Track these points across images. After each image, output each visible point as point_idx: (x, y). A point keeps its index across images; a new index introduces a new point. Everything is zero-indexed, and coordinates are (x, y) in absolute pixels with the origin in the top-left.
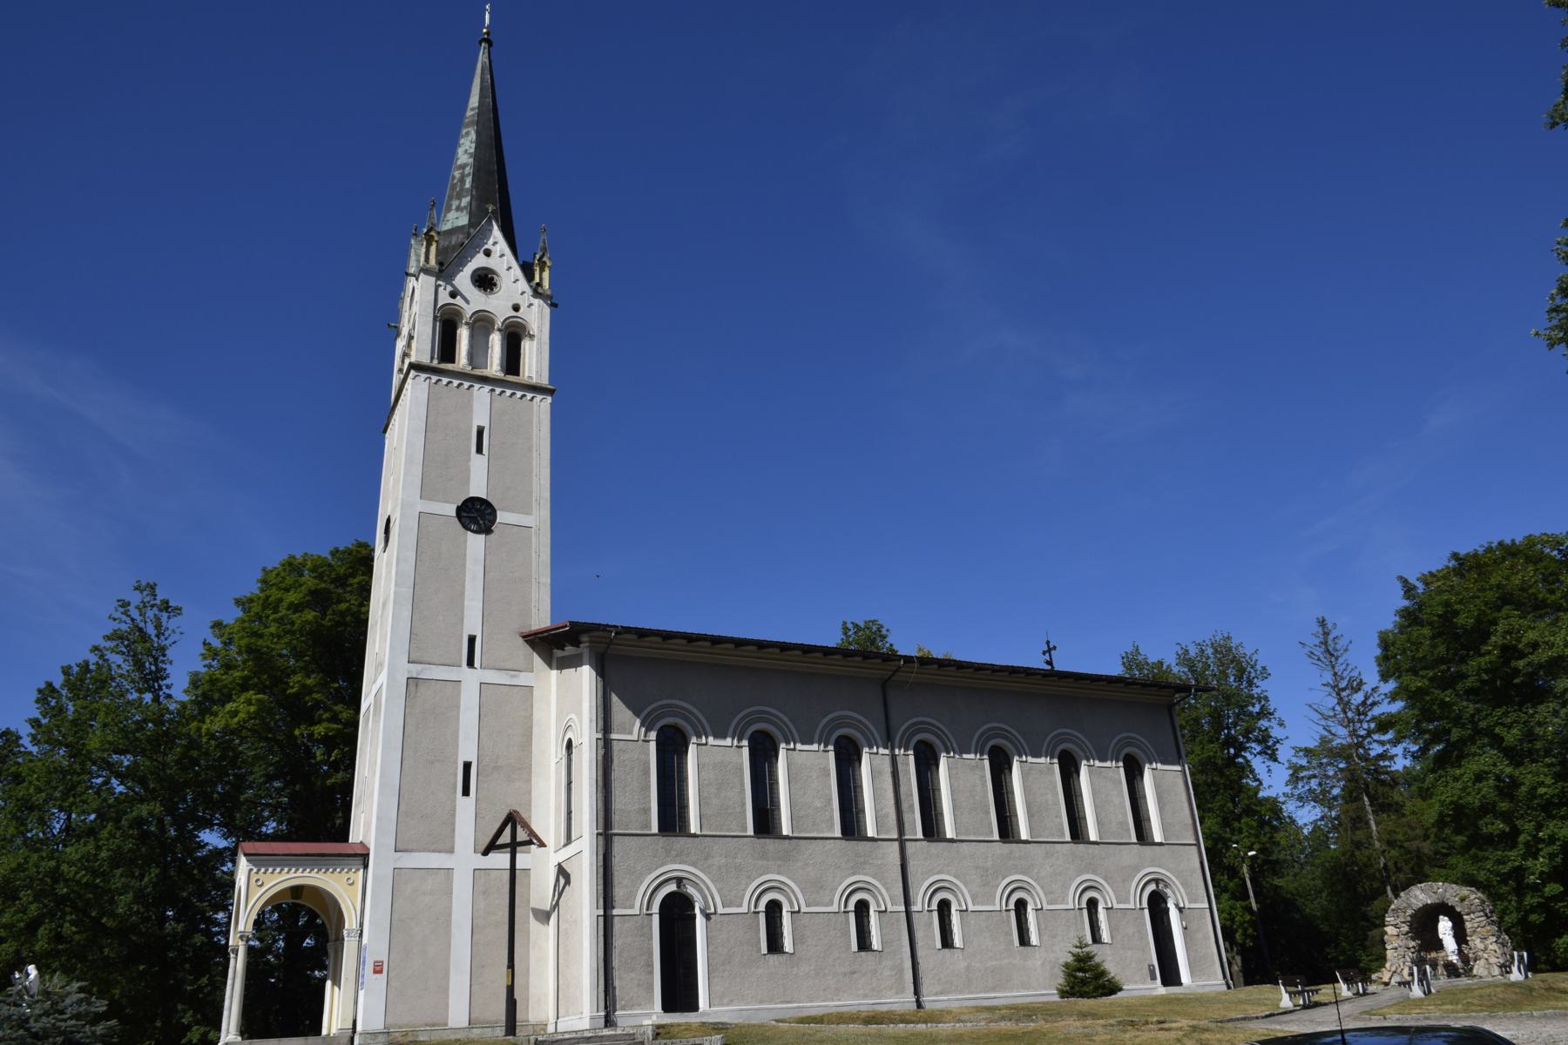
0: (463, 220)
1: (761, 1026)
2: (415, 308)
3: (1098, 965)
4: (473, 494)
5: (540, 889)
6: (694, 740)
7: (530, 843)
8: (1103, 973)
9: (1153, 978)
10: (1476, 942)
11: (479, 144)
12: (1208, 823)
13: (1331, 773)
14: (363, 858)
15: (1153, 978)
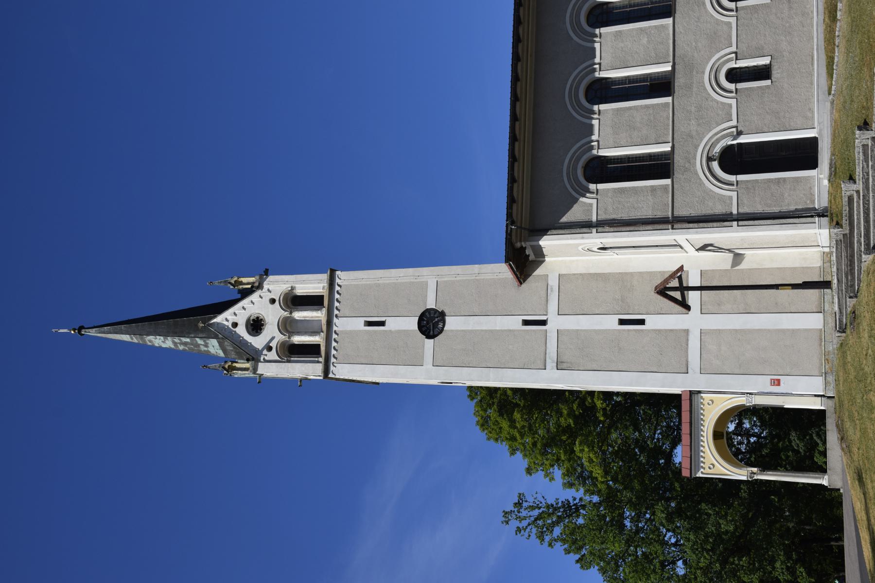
0: (214, 342)
4: (415, 327)
5: (719, 262)
6: (595, 152)
7: (680, 278)
11: (156, 333)
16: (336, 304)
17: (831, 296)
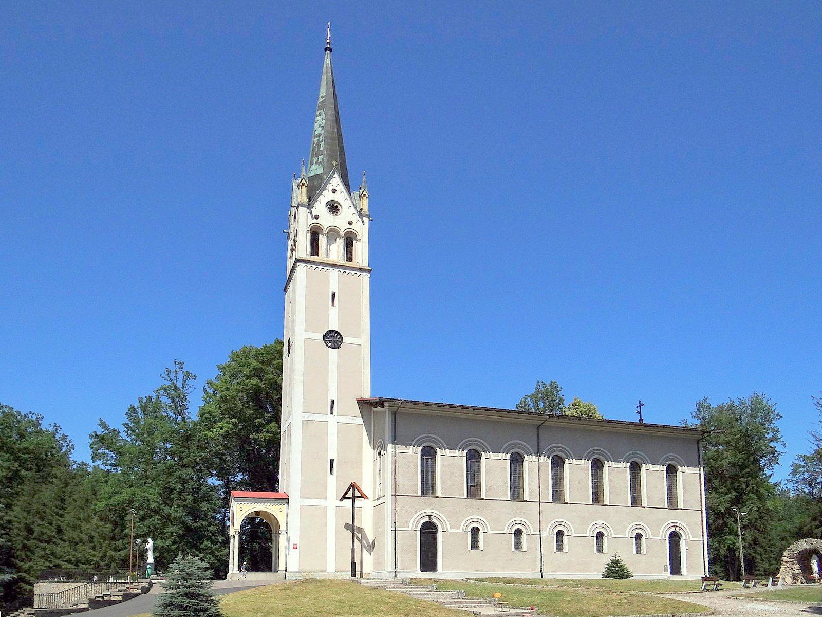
7: (362, 497)
14: (287, 501)
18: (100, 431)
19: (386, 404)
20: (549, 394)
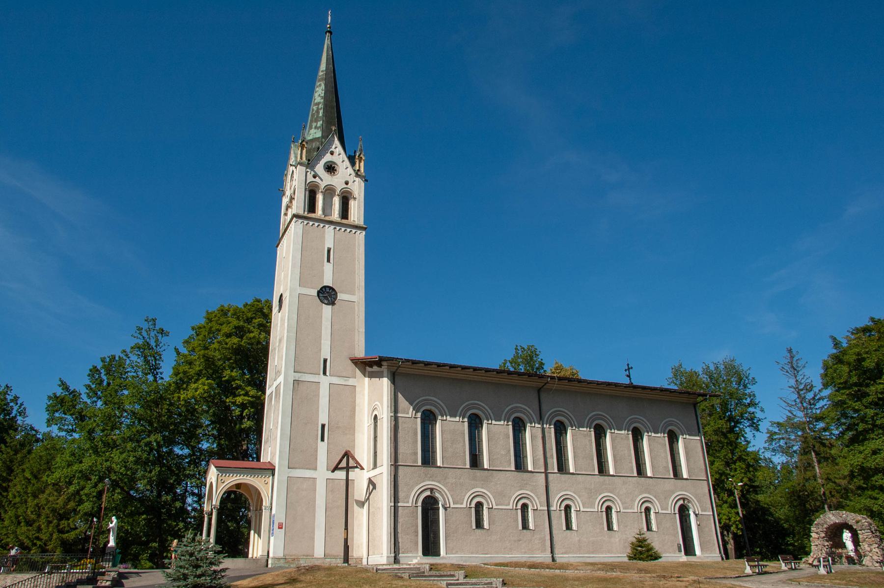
0: (319, 134)
1: (476, 566)
2: (294, 183)
3: (649, 544)
5: (360, 489)
6: (440, 417)
7: (356, 467)
8: (651, 549)
9: (680, 551)
10: (865, 546)
12: (717, 464)
13: (793, 437)
15: (680, 551)
16: (343, 229)
17: (340, 562)
18: (59, 392)
19: (384, 363)
20: (530, 356)
